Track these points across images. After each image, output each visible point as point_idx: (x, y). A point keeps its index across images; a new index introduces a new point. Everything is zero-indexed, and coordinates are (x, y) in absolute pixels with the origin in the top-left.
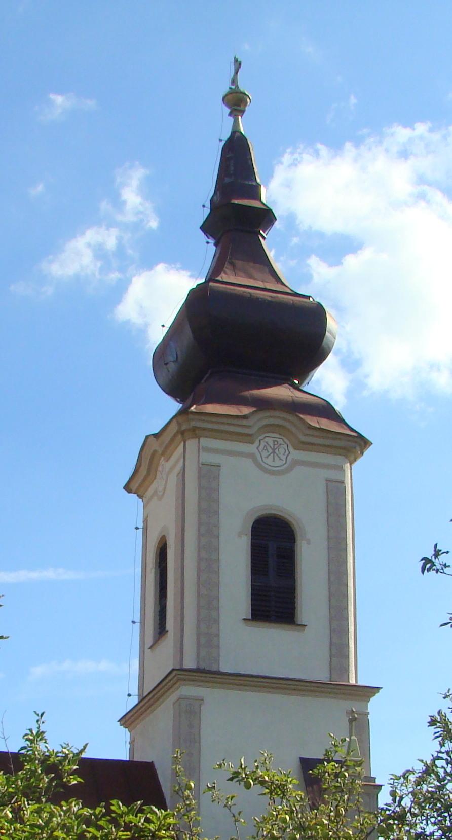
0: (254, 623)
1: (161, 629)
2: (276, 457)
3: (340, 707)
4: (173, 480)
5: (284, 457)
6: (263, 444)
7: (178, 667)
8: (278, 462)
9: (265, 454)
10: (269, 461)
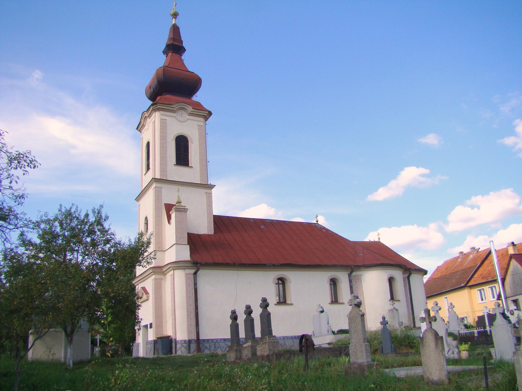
1: (148, 168)
3: (202, 192)
4: (151, 125)
7: (154, 178)
8: (183, 119)
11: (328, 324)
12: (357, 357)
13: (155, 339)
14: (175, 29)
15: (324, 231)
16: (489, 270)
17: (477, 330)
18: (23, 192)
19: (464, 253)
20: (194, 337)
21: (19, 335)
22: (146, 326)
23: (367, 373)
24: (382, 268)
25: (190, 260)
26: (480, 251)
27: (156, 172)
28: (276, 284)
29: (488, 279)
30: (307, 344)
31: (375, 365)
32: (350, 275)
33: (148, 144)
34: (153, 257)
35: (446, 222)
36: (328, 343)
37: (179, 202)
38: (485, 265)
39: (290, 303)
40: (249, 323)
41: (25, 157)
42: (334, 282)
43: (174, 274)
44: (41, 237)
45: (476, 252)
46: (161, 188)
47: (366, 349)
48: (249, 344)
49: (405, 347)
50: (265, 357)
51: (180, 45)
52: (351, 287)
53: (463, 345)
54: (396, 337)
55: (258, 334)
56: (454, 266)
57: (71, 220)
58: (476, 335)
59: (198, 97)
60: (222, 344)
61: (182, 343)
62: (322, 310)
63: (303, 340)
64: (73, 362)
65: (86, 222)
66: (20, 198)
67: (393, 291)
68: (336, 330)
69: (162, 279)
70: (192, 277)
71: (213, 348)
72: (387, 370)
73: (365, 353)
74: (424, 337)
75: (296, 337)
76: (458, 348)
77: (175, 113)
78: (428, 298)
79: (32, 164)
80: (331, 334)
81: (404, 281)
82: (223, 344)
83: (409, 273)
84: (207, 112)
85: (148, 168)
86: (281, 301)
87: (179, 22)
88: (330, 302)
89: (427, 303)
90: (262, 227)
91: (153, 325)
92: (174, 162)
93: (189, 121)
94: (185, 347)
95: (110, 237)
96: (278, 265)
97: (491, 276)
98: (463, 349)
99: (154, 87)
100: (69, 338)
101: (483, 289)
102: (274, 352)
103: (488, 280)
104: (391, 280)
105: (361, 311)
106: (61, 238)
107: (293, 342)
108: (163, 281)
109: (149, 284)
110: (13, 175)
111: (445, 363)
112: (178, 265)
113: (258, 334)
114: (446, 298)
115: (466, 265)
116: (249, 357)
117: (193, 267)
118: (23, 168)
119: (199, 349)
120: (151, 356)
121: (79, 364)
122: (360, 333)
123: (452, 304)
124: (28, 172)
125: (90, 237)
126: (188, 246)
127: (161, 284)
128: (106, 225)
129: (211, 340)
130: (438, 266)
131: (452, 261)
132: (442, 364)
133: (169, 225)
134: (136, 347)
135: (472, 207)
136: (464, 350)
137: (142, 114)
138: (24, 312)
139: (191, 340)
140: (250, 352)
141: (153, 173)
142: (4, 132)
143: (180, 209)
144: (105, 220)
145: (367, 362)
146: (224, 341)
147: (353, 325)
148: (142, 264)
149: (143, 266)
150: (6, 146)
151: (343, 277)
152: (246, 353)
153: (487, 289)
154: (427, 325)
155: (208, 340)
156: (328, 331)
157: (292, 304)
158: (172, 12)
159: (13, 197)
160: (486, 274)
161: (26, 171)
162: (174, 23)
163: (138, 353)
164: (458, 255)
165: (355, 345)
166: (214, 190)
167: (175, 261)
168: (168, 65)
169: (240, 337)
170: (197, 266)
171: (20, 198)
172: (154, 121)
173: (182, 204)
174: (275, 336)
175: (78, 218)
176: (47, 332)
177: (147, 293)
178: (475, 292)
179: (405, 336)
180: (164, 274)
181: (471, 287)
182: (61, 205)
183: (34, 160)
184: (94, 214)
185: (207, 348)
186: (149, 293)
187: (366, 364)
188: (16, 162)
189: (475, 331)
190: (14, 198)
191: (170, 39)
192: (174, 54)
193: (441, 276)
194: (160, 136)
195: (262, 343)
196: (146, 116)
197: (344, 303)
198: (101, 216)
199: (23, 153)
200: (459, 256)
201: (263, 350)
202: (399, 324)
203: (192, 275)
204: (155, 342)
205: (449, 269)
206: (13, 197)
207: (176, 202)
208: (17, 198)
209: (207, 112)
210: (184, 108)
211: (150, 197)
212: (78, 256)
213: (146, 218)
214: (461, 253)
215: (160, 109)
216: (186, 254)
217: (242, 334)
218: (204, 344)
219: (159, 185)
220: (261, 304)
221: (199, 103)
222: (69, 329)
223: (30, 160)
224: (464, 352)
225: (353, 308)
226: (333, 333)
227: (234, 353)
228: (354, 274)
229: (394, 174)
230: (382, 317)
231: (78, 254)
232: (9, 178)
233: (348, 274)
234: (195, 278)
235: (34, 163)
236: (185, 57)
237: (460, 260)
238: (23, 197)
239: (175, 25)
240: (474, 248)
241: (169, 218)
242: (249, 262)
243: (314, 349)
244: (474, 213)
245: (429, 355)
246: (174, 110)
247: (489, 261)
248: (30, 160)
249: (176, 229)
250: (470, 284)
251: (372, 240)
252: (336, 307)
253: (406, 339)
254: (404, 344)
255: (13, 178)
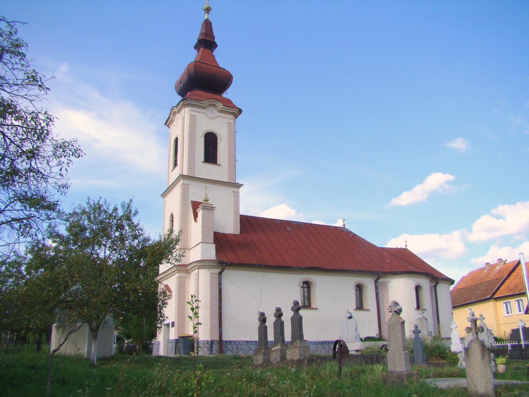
1: (176, 164)
3: (230, 190)
4: (180, 121)
11: (356, 330)
12: (396, 365)
13: (176, 338)
14: (208, 25)
15: (351, 235)
16: (517, 283)
17: (510, 344)
18: (66, 182)
19: (490, 264)
20: (217, 338)
21: (39, 328)
22: (168, 325)
23: (405, 382)
24: (409, 276)
25: (215, 259)
26: (507, 263)
27: (183, 168)
28: (301, 287)
29: (515, 292)
30: (341, 350)
31: (415, 375)
32: (376, 282)
33: (176, 140)
34: (182, 255)
35: (470, 230)
36: (356, 349)
37: (206, 200)
38: (512, 278)
39: (314, 308)
40: (279, 325)
41: (71, 145)
42: (359, 288)
43: (198, 272)
44: (69, 230)
45: (503, 263)
46: (188, 186)
47: (405, 358)
48: (278, 347)
49: (435, 358)
50: (296, 361)
51: (212, 40)
52: (377, 294)
53: (500, 358)
54: (426, 346)
55: (288, 337)
56: (480, 277)
57: (99, 215)
58: (509, 348)
59: (228, 94)
60: (245, 347)
61: (204, 343)
62: (350, 316)
63: (337, 345)
64: (97, 358)
65: (115, 217)
66: (63, 188)
67: (420, 300)
68: (363, 337)
69: (186, 278)
70: (217, 276)
71: (235, 350)
72: (428, 381)
73: (404, 362)
74: (470, 347)
75: (312, 343)
76: (495, 361)
77: (205, 109)
78: (454, 307)
79: (77, 153)
80: (359, 341)
81: (431, 290)
82: (246, 346)
83: (436, 282)
84: (237, 110)
85: (176, 164)
86: (306, 305)
87: (212, 17)
88: (355, 308)
89: (453, 313)
90: (289, 229)
91: (175, 324)
92: (203, 160)
93: (218, 118)
94: (207, 348)
95: (139, 232)
96: (304, 268)
97: (518, 289)
98: (500, 362)
99: (184, 83)
100: (94, 334)
101: (509, 302)
102: (304, 356)
103: (515, 293)
104: (418, 289)
105: (401, 318)
106: (88, 232)
107: (317, 347)
108: (187, 280)
109: (172, 282)
110: (63, 162)
111: (492, 376)
112: (203, 264)
113: (288, 337)
114: (470, 309)
115: (492, 277)
116: (278, 361)
117: (219, 267)
118: (67, 157)
119: (221, 351)
120: (172, 355)
121: (103, 360)
122: (400, 340)
123: (482, 316)
124: (72, 161)
125: (118, 231)
126: (214, 245)
127: (185, 282)
128: (135, 220)
129: (233, 342)
130: (463, 277)
131: (477, 272)
132: (489, 377)
133: (195, 223)
134: (156, 345)
135: (498, 217)
136: (501, 364)
137: (171, 109)
138: (51, 305)
139: (213, 341)
140: (279, 356)
141: (180, 170)
142: (55, 118)
143: (207, 207)
144: (134, 215)
145: (406, 371)
146: (246, 343)
147: (392, 332)
148: (170, 261)
149: (171, 264)
150: (52, 133)
151: (369, 283)
152: (275, 357)
153: (513, 302)
154: (473, 335)
155: (230, 342)
156: (356, 338)
157: (316, 309)
158: (205, 7)
159: (56, 186)
160: (514, 286)
161: (70, 160)
162: (206, 17)
163: (158, 351)
164: (484, 266)
165: (394, 354)
166: (241, 190)
167: (200, 259)
168: (200, 60)
169: (268, 340)
170: (222, 266)
171: (63, 188)
172: (184, 117)
173: (210, 202)
174: (305, 341)
175: (106, 212)
176: (81, 326)
177: (170, 291)
178: (501, 304)
179: (435, 346)
180: (188, 272)
181: (497, 299)
182: (89, 199)
183: (78, 149)
184: (123, 209)
185: (229, 349)
186: (172, 291)
187: (405, 373)
188: (61, 150)
189: (509, 345)
190: (57, 187)
191: (201, 34)
192: (205, 50)
193: (466, 287)
194: (189, 132)
195: (292, 348)
196: (175, 111)
197: (369, 310)
198: (131, 211)
199: (69, 141)
200: (485, 268)
201: (293, 354)
202: (427, 333)
203: (216, 275)
204: (177, 341)
205: (474, 279)
206: (56, 186)
207: (203, 200)
208: (60, 188)
209: (237, 110)
210: (214, 105)
211: (176, 193)
212: (106, 251)
213: (172, 215)
214: (488, 264)
215: (190, 105)
216: (211, 253)
217: (271, 337)
218: (226, 345)
219: (186, 182)
220: (292, 307)
221: (230, 100)
222: (94, 324)
223: (74, 149)
224: (501, 365)
225: (393, 315)
226: (361, 339)
227: (262, 357)
228: (380, 280)
229: (421, 179)
230: (414, 325)
231: (105, 249)
232: (59, 166)
233: (375, 280)
234: (220, 277)
235: (79, 152)
236: (216, 53)
237: (485, 271)
238: (66, 187)
239: (208, 20)
240: (501, 260)
241: (196, 216)
242: (274, 264)
243: (348, 355)
244: (499, 223)
245: (475, 367)
246: (204, 107)
247: (516, 274)
248: (74, 149)
249: (203, 227)
250: (496, 296)
251: (399, 247)
252: (360, 313)
253: (437, 349)
254: (435, 354)
255: (63, 165)
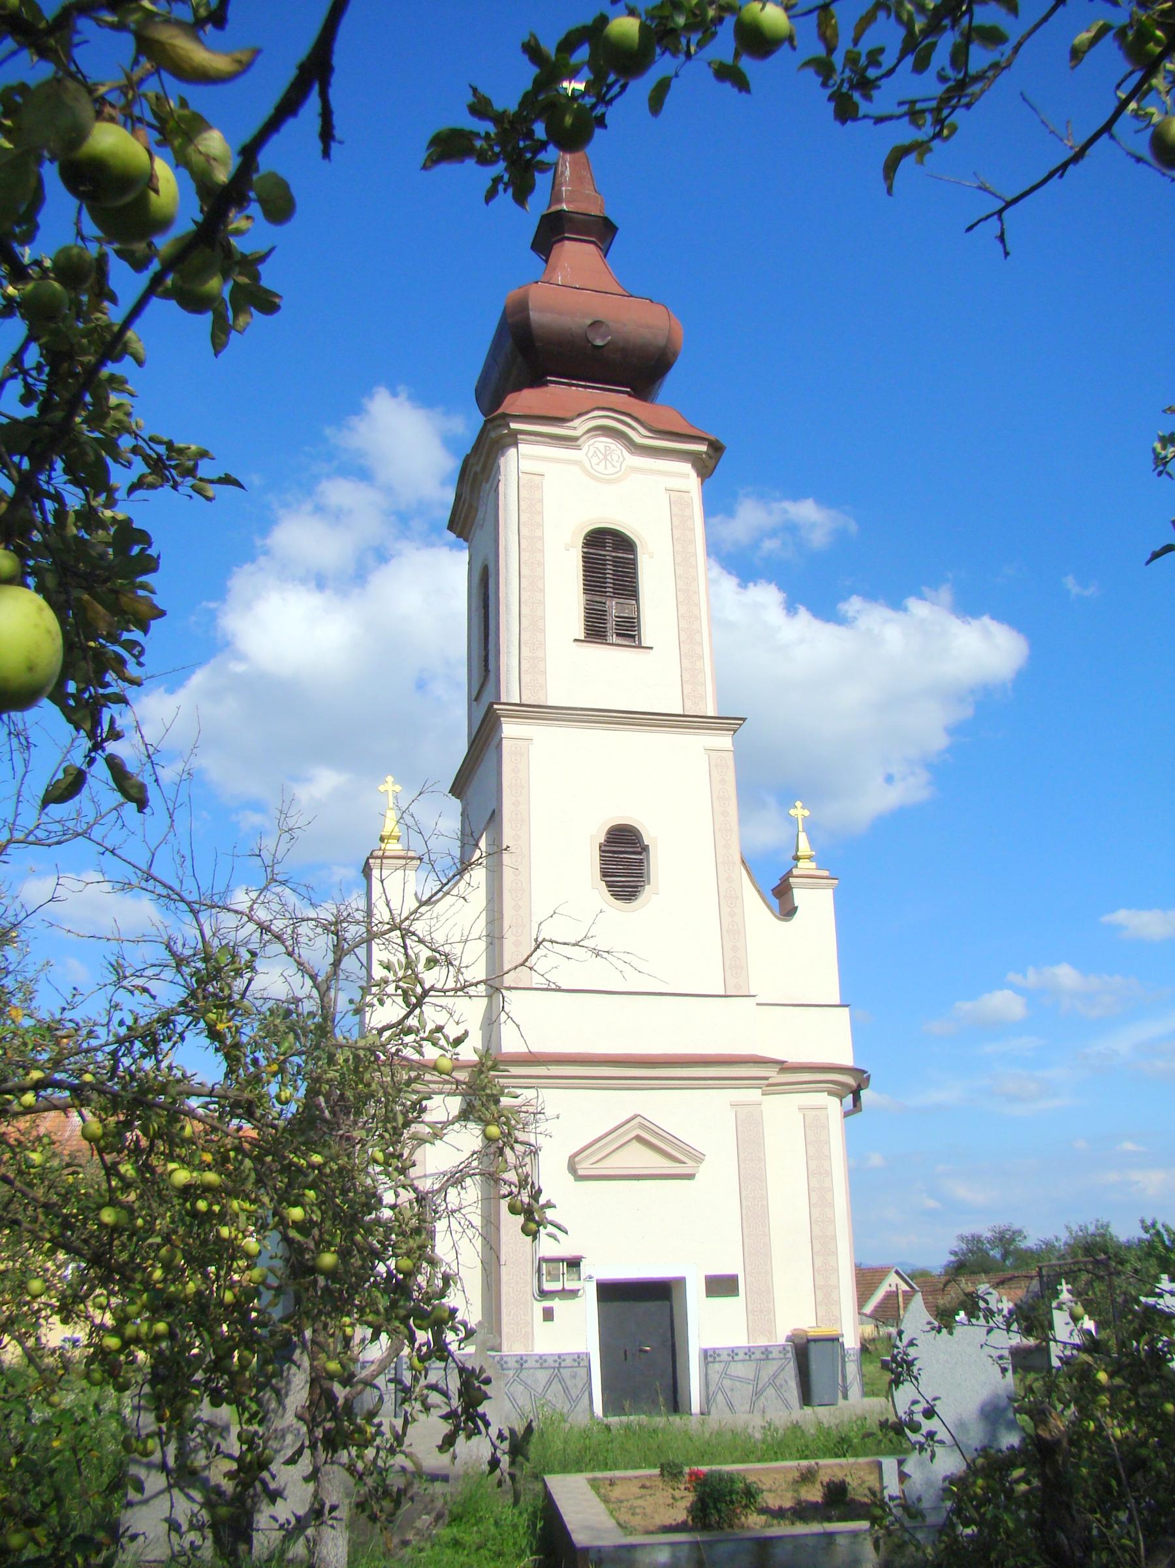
0: (674, 1296)
2: (609, 465)
5: (618, 465)
6: (592, 449)
9: (595, 460)
10: (601, 468)
